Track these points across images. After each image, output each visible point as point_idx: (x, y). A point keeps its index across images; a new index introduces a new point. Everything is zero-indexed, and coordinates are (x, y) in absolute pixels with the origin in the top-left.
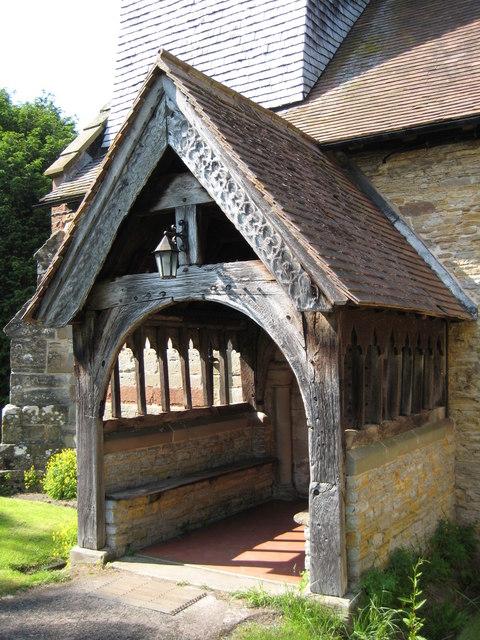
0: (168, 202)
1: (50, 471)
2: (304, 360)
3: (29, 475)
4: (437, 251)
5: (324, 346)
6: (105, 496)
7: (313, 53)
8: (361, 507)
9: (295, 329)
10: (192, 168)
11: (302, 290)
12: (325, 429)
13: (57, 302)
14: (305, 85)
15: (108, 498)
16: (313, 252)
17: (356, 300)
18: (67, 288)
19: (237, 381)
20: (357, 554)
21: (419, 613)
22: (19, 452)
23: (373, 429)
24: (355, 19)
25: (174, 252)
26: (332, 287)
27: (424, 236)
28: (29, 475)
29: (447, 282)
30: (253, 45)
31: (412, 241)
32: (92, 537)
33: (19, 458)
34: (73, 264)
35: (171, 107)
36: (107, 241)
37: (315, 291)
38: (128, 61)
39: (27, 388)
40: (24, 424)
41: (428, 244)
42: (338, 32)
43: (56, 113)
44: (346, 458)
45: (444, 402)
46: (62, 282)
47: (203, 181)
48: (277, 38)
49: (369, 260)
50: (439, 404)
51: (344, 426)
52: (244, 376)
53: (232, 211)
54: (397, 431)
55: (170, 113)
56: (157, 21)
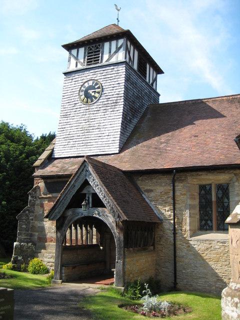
0: (84, 191)
1: (30, 265)
2: (116, 232)
3: (23, 266)
4: (153, 203)
5: (120, 229)
6: (62, 266)
7: (122, 137)
8: (128, 267)
9: (114, 225)
10: (92, 185)
11: (116, 217)
12: (120, 248)
13: (54, 214)
14: (119, 148)
15: (63, 266)
16: (119, 208)
17: (128, 220)
18: (57, 211)
19: (95, 237)
20: (126, 277)
21: (139, 290)
22: (20, 258)
23: (131, 249)
24: (136, 123)
25: (86, 205)
26: (123, 216)
27: (150, 199)
28: (23, 266)
29: (155, 212)
30: (105, 132)
31: (147, 200)
32: (58, 276)
33: (19, 260)
34: (59, 204)
35: (87, 169)
36: (69, 200)
37: (119, 217)
38: (62, 130)
39: (23, 237)
40: (22, 249)
41: (151, 201)
42: (131, 127)
43: (26, 132)
44: (124, 255)
45: (153, 245)
46: (56, 209)
47: (94, 188)
48: (112, 131)
49: (132, 209)
50: (152, 246)
51: (124, 247)
52: (97, 236)
53: (101, 197)
54: (138, 251)
55: (87, 171)
56: (73, 118)
